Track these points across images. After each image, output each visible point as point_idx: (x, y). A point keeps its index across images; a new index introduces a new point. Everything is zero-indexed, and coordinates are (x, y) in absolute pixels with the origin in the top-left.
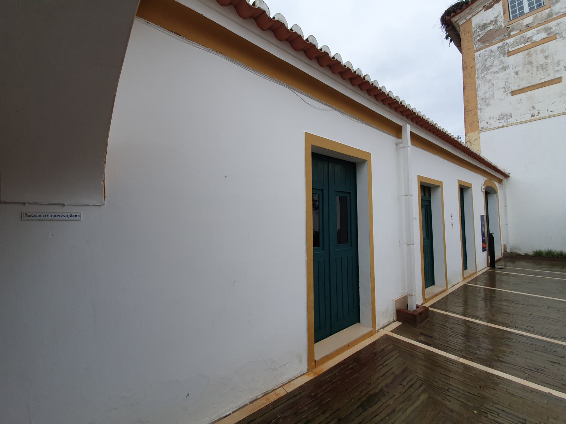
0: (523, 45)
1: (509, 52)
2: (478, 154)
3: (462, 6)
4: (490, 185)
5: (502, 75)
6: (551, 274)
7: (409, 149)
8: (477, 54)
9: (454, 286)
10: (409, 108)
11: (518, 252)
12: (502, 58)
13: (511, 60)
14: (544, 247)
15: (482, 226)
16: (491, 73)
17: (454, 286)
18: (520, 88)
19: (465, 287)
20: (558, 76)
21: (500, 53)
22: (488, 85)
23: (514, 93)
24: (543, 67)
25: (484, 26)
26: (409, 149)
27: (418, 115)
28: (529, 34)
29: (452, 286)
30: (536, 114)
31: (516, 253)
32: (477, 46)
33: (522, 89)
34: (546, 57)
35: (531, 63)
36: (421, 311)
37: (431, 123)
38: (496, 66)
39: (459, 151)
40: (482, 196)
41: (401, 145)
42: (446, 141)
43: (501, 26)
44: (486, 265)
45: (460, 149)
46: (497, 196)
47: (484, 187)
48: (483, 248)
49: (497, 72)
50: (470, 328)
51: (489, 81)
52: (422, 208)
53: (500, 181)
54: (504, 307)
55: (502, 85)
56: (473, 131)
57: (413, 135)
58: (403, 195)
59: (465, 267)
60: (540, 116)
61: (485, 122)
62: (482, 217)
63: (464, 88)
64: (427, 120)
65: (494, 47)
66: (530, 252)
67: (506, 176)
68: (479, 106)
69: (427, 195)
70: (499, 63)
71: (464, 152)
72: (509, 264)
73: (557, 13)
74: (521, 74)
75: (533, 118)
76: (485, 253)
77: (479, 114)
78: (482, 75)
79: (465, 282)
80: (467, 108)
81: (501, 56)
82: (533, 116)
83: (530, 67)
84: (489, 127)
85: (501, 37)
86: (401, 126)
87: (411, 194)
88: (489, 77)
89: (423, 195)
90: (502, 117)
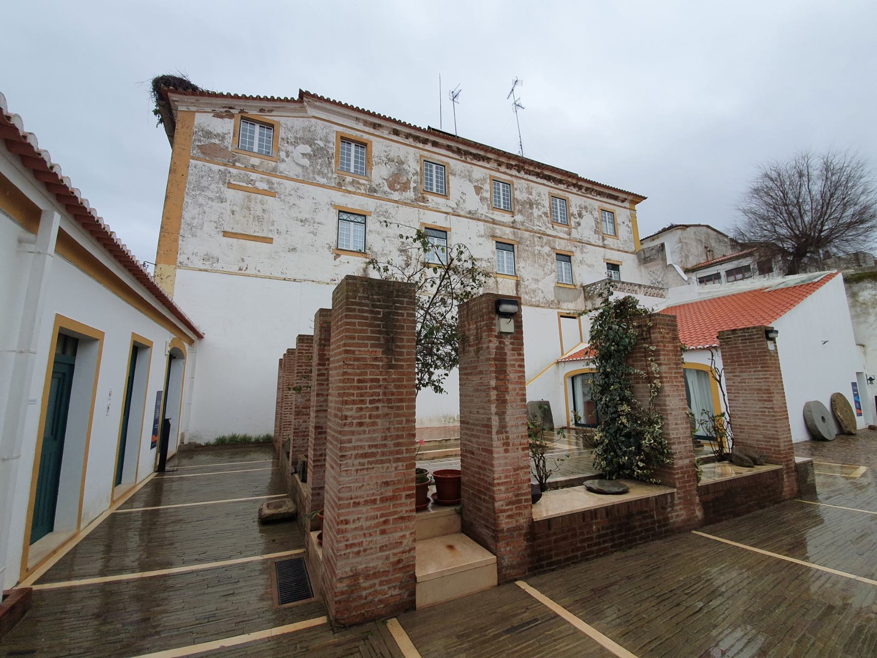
0: (245, 185)
1: (229, 183)
2: (170, 299)
3: (188, 88)
4: (177, 346)
5: (216, 205)
6: (232, 466)
7: (49, 260)
8: (193, 162)
9: (92, 522)
10: (68, 185)
11: (198, 442)
12: (221, 185)
13: (230, 194)
14: (227, 431)
15: (157, 407)
16: (205, 196)
17: (92, 522)
18: (234, 231)
19: (113, 516)
20: (270, 236)
21: (220, 179)
22: (197, 210)
23: (226, 234)
24: (259, 219)
25: (208, 134)
26: (49, 260)
27: (82, 203)
28: (254, 176)
29: (89, 524)
30: (244, 268)
31: (195, 444)
32: (195, 152)
33: (235, 234)
34: (264, 211)
35: (249, 209)
36: (14, 603)
37: (104, 228)
38: (212, 192)
39: (143, 287)
40: (165, 360)
41: (33, 246)
42: (125, 266)
43: (227, 147)
44: (152, 470)
45: (144, 285)
46: (185, 363)
47: (169, 349)
48: (152, 443)
49: (212, 200)
50: (112, 593)
51: (201, 205)
52: (52, 377)
53: (191, 342)
54: (167, 535)
55: (215, 218)
56: (166, 262)
57: (62, 237)
58: (14, 351)
59: (118, 480)
60: (247, 272)
61: (186, 257)
62: (159, 393)
63: (166, 198)
64: (98, 221)
65: (216, 167)
66: (211, 439)
67: (200, 336)
68: (182, 232)
69: (69, 352)
70: (216, 190)
71: (151, 291)
72: (184, 461)
73: (281, 172)
74: (238, 216)
75: (240, 272)
76: (155, 449)
77: (180, 242)
78: (194, 193)
79: (113, 510)
80: (165, 227)
81: (221, 183)
82: (240, 269)
83: (247, 212)
84: (190, 265)
85: (225, 161)
86: (41, 211)
87: (32, 350)
88: (201, 200)
89: (60, 352)
90: (207, 258)
